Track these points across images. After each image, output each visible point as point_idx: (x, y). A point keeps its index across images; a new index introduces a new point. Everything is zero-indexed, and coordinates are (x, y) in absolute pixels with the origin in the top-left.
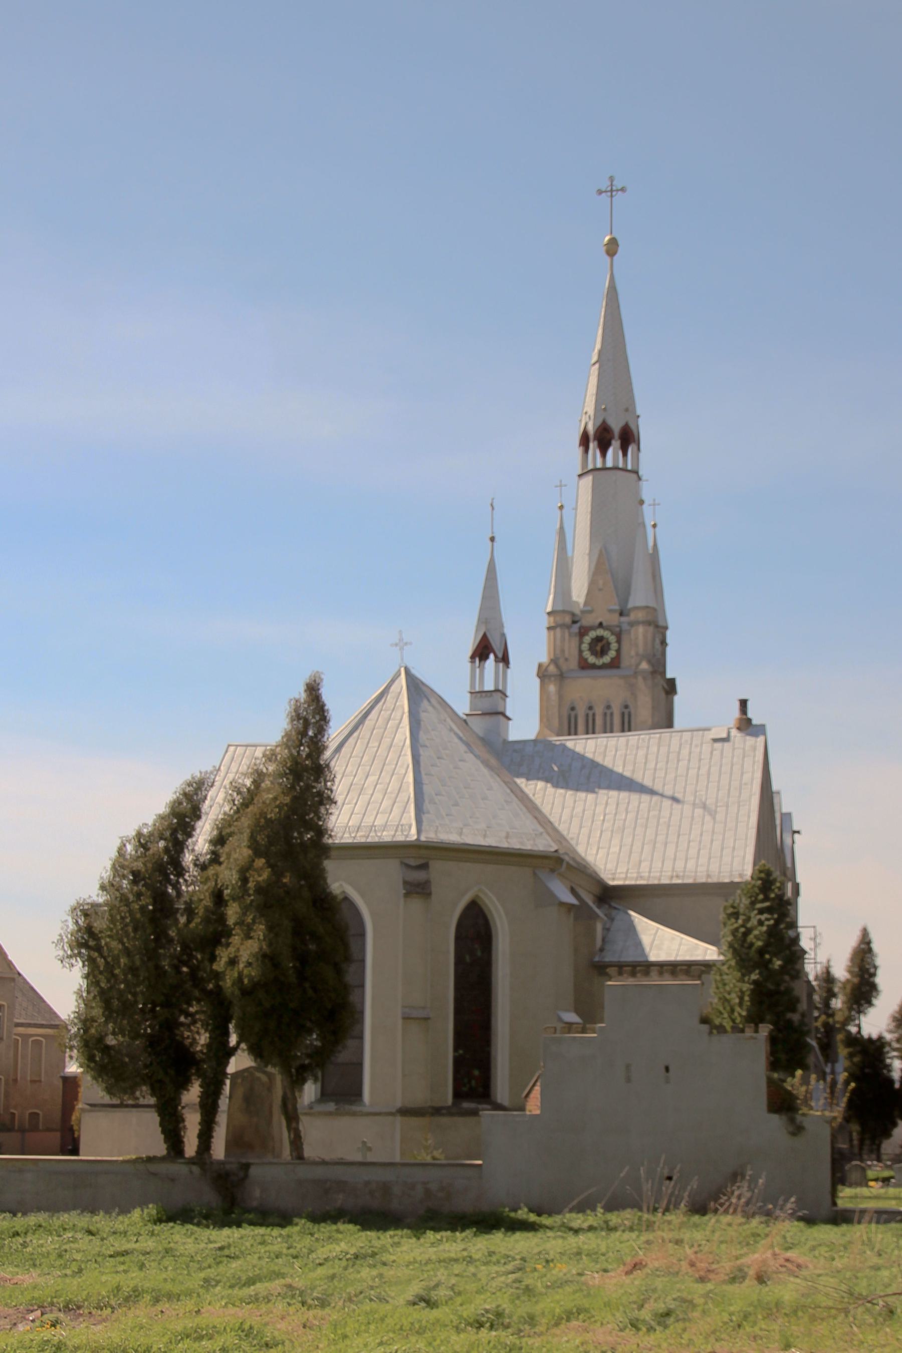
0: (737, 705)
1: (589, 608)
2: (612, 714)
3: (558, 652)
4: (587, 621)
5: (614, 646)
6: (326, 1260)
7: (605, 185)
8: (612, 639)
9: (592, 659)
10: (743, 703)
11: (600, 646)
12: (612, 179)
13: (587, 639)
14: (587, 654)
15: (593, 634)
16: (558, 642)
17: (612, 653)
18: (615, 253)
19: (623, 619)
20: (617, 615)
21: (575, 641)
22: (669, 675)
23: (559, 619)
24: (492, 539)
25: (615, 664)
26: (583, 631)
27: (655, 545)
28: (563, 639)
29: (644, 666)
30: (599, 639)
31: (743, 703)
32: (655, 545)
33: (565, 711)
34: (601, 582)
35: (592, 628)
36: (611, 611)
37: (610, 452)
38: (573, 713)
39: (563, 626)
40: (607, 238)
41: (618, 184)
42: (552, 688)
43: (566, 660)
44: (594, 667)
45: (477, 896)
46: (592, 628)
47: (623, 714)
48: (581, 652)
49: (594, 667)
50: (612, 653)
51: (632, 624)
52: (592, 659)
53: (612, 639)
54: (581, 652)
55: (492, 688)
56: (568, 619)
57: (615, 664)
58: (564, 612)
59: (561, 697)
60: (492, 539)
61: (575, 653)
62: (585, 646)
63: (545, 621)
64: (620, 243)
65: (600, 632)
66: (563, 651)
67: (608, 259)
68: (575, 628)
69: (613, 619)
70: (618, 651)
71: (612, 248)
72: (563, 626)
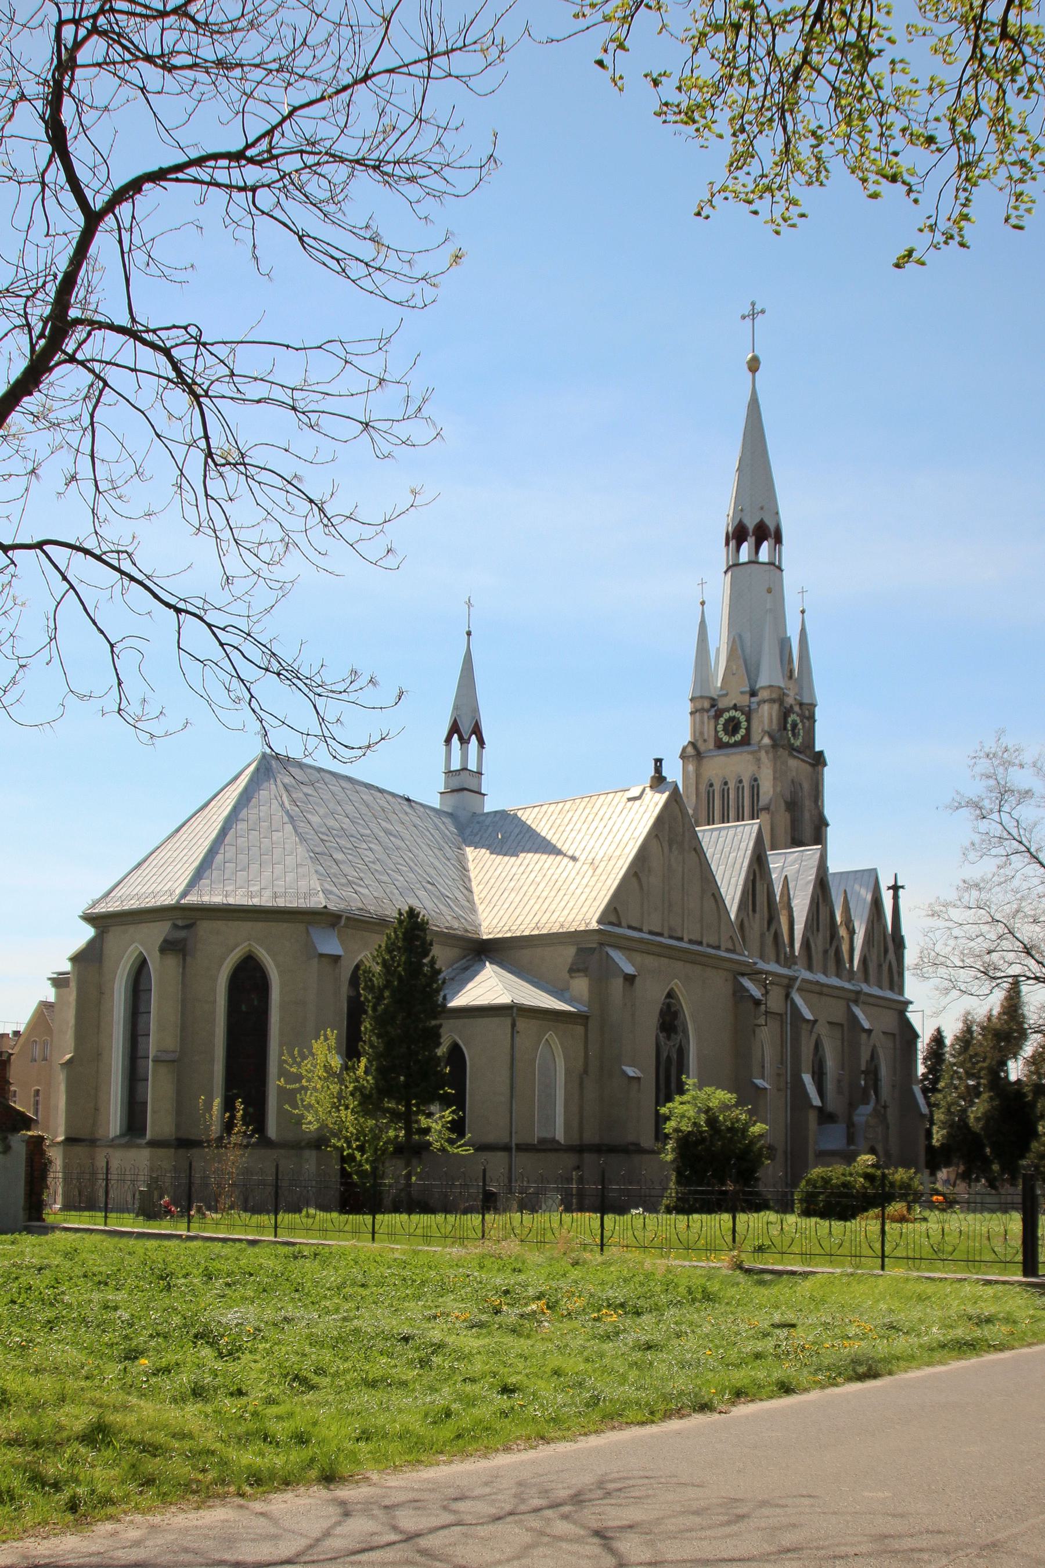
0: (652, 765)
1: (724, 692)
2: (743, 787)
3: (697, 734)
4: (721, 705)
5: (744, 724)
6: (383, 1379)
7: (747, 310)
8: (743, 718)
9: (725, 739)
10: (658, 762)
11: (733, 726)
12: (753, 304)
13: (722, 721)
14: (721, 734)
15: (726, 715)
16: (697, 726)
17: (743, 732)
18: (757, 369)
19: (754, 699)
20: (747, 697)
21: (712, 722)
22: (817, 749)
23: (699, 706)
24: (469, 634)
25: (746, 741)
26: (718, 715)
27: (803, 632)
28: (702, 723)
29: (766, 741)
30: (732, 719)
31: (658, 762)
32: (803, 632)
33: (703, 788)
34: (734, 667)
35: (728, 710)
36: (742, 693)
37: (745, 546)
38: (711, 789)
39: (702, 710)
40: (750, 356)
41: (758, 308)
42: (691, 768)
43: (705, 741)
44: (728, 745)
45: (250, 950)
46: (728, 710)
47: (753, 787)
48: (716, 732)
49: (728, 745)
50: (743, 732)
51: (759, 704)
52: (725, 739)
53: (743, 718)
54: (716, 732)
55: (459, 768)
56: (706, 704)
57: (746, 741)
58: (702, 697)
59: (698, 776)
60: (469, 634)
61: (713, 733)
62: (720, 727)
63: (688, 707)
64: (761, 360)
65: (733, 713)
66: (702, 733)
67: (750, 374)
68: (712, 713)
69: (744, 700)
70: (748, 729)
71: (754, 365)
72: (702, 710)
